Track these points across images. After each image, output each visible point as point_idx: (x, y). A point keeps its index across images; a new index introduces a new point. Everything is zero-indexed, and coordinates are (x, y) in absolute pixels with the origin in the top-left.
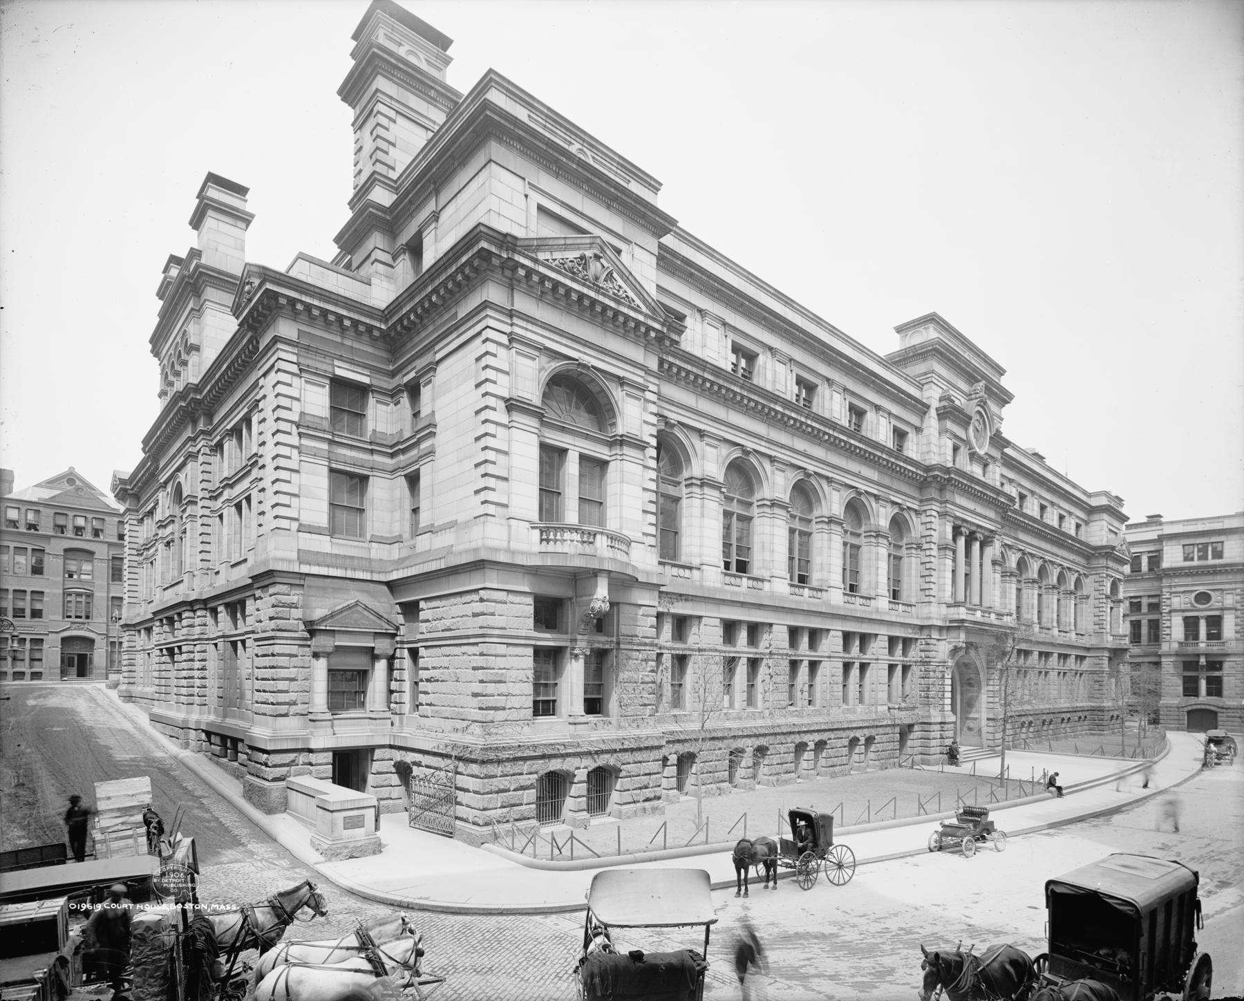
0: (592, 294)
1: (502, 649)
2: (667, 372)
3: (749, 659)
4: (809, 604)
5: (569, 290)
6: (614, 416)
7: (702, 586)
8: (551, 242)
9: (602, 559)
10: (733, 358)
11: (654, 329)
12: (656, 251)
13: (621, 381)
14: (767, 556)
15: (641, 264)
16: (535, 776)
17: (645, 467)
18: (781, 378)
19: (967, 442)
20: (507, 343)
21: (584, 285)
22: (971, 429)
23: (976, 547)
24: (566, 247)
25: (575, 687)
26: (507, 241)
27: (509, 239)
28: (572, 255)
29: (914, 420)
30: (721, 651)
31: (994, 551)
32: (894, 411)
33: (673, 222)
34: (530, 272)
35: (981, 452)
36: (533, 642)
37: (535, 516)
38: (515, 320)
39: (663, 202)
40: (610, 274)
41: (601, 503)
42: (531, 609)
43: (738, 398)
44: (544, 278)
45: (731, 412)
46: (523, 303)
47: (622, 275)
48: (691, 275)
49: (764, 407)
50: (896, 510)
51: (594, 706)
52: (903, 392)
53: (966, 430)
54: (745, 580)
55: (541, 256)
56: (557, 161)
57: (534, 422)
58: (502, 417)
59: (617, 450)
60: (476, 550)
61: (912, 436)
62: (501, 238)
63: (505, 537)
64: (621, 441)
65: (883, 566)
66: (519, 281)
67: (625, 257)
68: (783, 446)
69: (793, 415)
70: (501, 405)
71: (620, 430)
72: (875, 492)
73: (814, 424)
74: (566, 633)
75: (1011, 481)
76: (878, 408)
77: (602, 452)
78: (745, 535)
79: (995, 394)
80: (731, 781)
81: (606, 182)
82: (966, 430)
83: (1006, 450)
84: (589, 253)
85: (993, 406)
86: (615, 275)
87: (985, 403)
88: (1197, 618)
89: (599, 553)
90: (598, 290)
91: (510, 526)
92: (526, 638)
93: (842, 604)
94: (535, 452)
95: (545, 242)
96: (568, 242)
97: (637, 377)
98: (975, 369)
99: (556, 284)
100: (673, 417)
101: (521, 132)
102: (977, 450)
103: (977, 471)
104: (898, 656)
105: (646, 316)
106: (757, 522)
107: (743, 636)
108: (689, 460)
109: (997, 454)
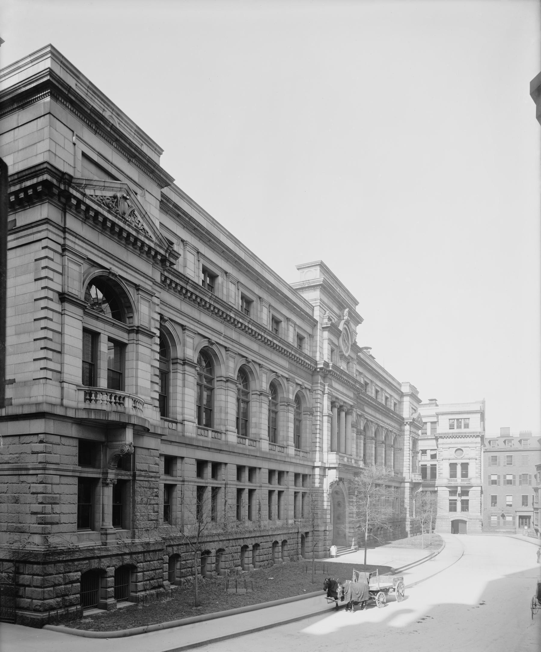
0: (121, 224)
1: (56, 479)
2: (166, 284)
3: (165, 485)
4: (249, 450)
5: (105, 219)
6: (132, 312)
7: (183, 436)
8: (95, 183)
9: (130, 416)
10: (202, 276)
11: (160, 254)
12: (160, 198)
13: (137, 288)
14: (223, 416)
15: (149, 203)
16: (79, 573)
17: (152, 350)
18: (233, 294)
19: (338, 347)
20: (60, 250)
21: (116, 217)
22: (341, 339)
23: (343, 414)
24: (104, 188)
25: (106, 508)
26: (65, 178)
27: (67, 177)
28: (109, 194)
29: (309, 330)
30: (195, 482)
31: (352, 418)
32: (297, 323)
33: (172, 180)
34: (79, 202)
35: (347, 355)
36: (78, 474)
37: (79, 381)
38: (68, 236)
39: (165, 163)
40: (133, 211)
41: (122, 374)
42: (76, 451)
43: (208, 306)
44: (88, 208)
45: (202, 314)
46: (73, 223)
47: (140, 213)
48: (178, 216)
49: (220, 312)
50: (243, 362)
51: (119, 519)
52: (303, 311)
53: (338, 339)
54: (210, 432)
55: (88, 192)
56: (96, 123)
57: (80, 311)
58: (57, 306)
59: (133, 336)
60: (38, 404)
61: (307, 340)
62: (61, 175)
63: (58, 395)
64: (138, 330)
65: (291, 425)
66: (70, 207)
67: (139, 197)
68: (194, 319)
69: (241, 320)
70: (56, 297)
71: (136, 323)
72: (287, 376)
73: (253, 328)
74: (99, 468)
75: (360, 373)
76: (288, 319)
77: (122, 336)
78: (210, 399)
79: (354, 317)
80: (242, 565)
81: (129, 144)
82: (338, 339)
83: (359, 354)
84: (119, 195)
85: (352, 324)
86: (136, 213)
87: (349, 323)
88: (456, 464)
89: (127, 411)
90: (125, 222)
91: (62, 388)
92: (73, 471)
93: (268, 450)
94: (79, 334)
95: (91, 183)
96: (107, 184)
97: (147, 285)
98: (343, 300)
99: (97, 213)
100: (167, 315)
101: (73, 98)
102: (345, 353)
103: (343, 366)
104: (208, 480)
105: (155, 244)
106: (217, 392)
107: (209, 470)
108: (174, 345)
109: (354, 356)
